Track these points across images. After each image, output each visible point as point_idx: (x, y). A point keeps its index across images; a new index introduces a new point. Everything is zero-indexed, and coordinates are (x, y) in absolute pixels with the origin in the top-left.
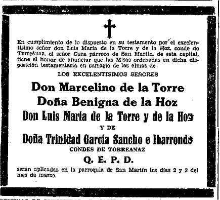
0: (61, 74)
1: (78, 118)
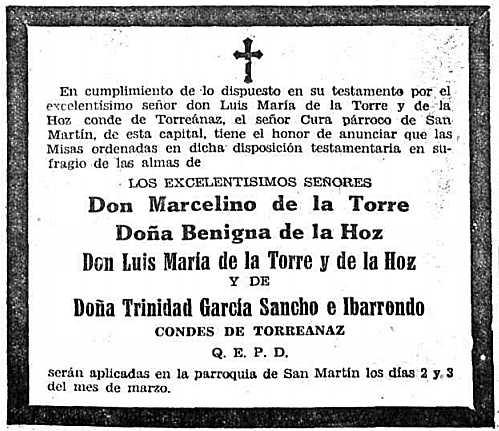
0: (134, 183)
1: (194, 265)
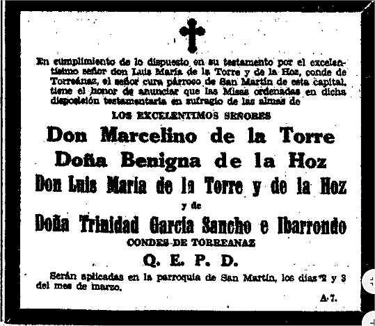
1: (133, 189)
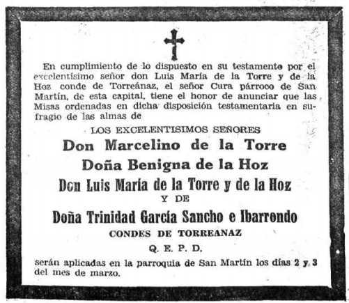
0: (95, 130)
1: (137, 187)
